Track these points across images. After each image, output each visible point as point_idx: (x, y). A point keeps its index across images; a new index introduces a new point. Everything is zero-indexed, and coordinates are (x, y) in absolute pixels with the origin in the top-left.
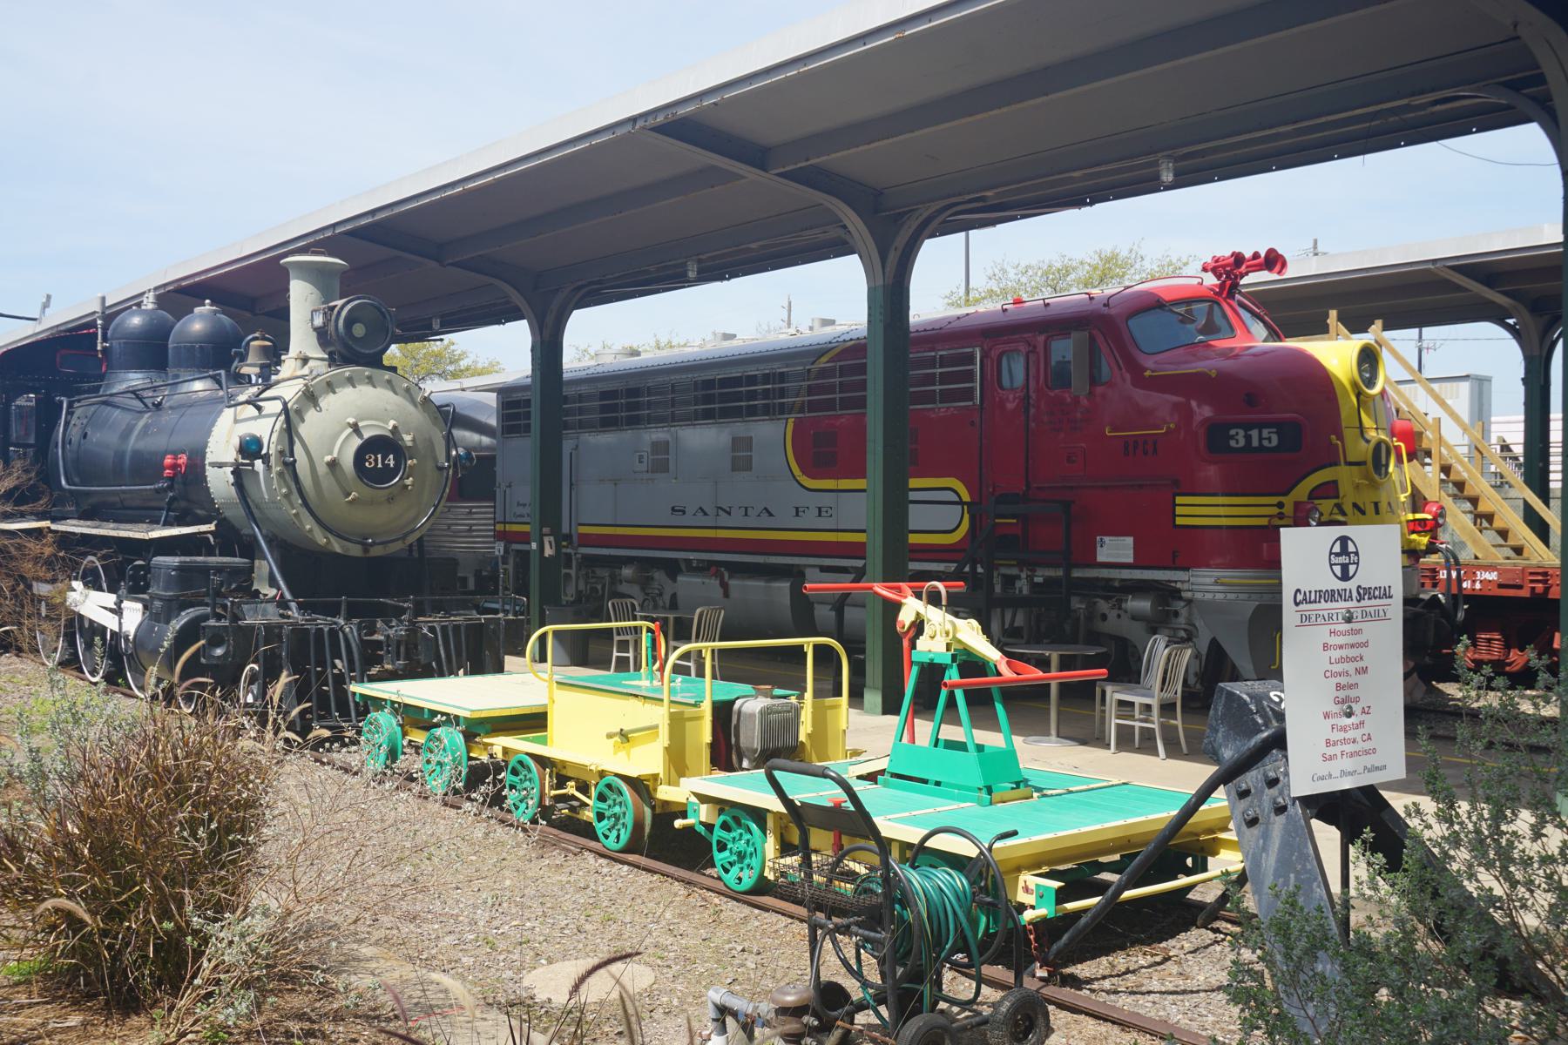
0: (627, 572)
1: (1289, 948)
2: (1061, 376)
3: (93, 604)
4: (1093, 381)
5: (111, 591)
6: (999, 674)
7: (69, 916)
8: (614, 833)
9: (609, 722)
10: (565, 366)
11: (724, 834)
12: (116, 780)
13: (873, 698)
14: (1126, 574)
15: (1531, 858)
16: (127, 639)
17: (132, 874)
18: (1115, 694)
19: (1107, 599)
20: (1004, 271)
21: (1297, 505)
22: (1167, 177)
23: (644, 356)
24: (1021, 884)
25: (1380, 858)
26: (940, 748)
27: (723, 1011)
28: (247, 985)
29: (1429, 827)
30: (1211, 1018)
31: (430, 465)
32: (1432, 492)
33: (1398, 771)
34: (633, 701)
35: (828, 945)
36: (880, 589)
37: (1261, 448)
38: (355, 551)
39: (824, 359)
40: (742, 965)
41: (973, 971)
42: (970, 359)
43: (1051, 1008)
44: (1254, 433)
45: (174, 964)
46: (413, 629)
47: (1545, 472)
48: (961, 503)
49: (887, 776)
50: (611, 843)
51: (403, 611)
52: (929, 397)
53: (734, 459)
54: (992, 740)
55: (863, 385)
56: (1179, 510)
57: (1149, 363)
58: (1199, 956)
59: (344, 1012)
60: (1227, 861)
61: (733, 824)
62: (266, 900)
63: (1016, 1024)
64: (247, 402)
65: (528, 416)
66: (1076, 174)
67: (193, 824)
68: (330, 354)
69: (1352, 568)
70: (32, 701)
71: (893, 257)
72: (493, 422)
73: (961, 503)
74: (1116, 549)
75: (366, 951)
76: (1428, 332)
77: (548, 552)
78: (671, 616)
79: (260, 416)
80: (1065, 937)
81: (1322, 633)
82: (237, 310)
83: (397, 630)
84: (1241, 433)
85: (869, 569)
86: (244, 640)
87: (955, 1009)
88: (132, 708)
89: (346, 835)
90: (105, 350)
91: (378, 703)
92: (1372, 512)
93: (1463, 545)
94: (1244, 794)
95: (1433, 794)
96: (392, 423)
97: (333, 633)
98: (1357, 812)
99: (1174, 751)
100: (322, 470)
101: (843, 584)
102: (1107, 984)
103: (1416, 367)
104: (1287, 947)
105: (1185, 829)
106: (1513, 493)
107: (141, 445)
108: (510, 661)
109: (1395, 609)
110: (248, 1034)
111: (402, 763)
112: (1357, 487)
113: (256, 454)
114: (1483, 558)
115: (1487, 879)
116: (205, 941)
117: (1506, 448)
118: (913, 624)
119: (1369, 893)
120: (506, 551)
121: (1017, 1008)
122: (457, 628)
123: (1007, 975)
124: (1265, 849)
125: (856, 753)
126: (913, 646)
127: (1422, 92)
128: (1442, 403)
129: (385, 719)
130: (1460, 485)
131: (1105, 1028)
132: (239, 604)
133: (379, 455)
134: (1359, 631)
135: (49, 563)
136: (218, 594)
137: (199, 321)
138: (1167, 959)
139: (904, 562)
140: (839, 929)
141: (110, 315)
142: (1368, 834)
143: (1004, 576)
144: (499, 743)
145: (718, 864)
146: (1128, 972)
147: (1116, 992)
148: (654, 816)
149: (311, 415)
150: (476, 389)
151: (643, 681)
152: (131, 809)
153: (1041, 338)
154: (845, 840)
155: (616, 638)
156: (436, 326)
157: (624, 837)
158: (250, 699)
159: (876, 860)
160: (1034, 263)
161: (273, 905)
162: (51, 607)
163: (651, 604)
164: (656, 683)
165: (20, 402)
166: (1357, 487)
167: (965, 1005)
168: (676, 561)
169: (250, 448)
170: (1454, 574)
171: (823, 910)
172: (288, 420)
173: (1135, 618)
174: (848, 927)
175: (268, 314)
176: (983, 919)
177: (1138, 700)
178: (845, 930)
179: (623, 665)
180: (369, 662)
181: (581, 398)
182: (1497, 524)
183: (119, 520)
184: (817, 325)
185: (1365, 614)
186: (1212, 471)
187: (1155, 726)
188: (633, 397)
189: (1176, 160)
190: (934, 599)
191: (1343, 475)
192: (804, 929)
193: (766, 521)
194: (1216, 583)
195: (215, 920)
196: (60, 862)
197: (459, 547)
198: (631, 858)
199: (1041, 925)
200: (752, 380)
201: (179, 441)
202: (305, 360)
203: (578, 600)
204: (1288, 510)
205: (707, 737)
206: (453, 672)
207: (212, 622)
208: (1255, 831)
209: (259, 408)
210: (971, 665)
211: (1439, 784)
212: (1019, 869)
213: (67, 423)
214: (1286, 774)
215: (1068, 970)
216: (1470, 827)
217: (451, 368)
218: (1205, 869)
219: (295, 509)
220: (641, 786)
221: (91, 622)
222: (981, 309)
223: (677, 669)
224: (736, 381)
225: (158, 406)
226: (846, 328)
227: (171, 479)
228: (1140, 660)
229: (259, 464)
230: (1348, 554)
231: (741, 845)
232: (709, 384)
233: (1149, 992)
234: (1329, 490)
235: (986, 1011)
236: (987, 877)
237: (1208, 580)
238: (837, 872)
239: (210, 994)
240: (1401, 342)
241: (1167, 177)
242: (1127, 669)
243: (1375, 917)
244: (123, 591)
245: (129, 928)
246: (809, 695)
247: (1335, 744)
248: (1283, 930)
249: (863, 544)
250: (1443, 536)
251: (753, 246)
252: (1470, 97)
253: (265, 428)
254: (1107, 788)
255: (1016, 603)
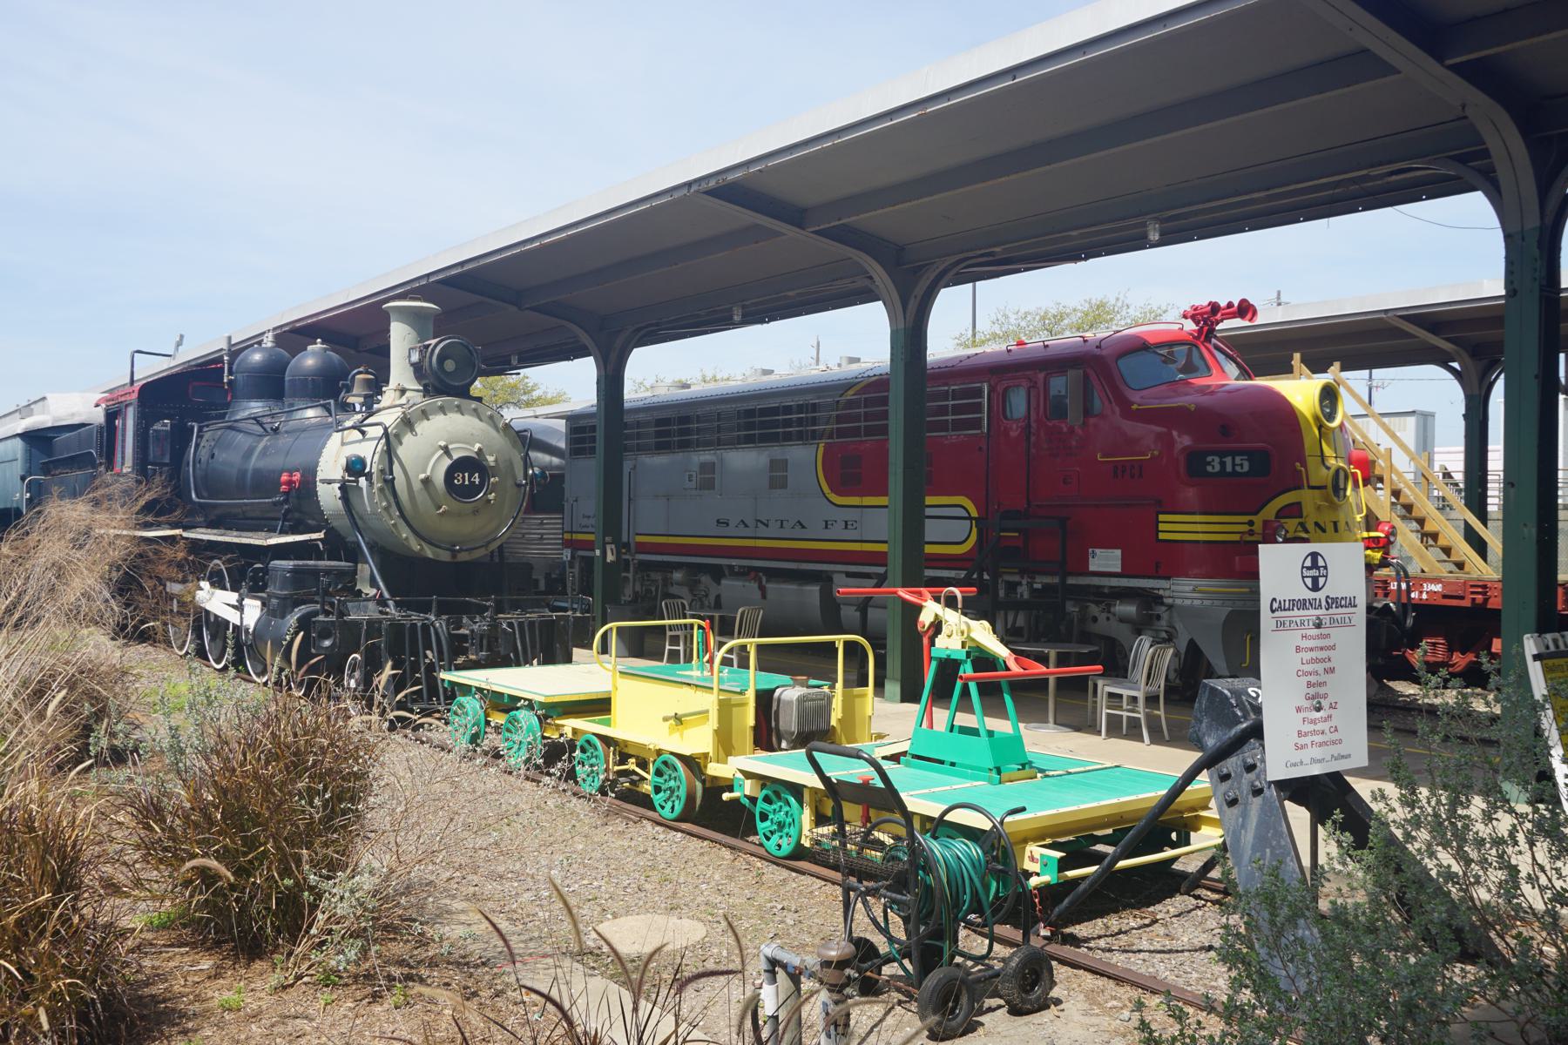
0: (677, 576)
1: (1273, 915)
2: (1059, 409)
3: (217, 601)
4: (1087, 412)
5: (233, 590)
6: (1008, 669)
7: (203, 872)
8: (670, 804)
9: (666, 707)
10: (626, 397)
11: (766, 806)
12: (244, 755)
13: (893, 688)
14: (1115, 582)
15: (1483, 840)
16: (247, 630)
17: (256, 837)
18: (1105, 687)
19: (1097, 603)
20: (1007, 317)
21: (1266, 523)
22: (1154, 236)
23: (693, 388)
24: (1027, 854)
25: (1348, 838)
26: (955, 734)
27: (774, 963)
28: (356, 935)
29: (1393, 810)
30: (1195, 975)
31: (510, 483)
32: (1384, 513)
33: (1361, 759)
34: (686, 689)
35: (859, 905)
36: (903, 593)
37: (1234, 473)
38: (445, 556)
39: (851, 392)
40: (782, 922)
41: (986, 930)
42: (979, 393)
43: (1054, 963)
44: (1228, 460)
45: (293, 915)
46: (494, 625)
47: (1483, 497)
48: (970, 518)
49: (908, 757)
50: (666, 813)
51: (486, 609)
52: (943, 426)
53: (771, 478)
54: (1001, 726)
55: (885, 415)
56: (1162, 527)
57: (1135, 397)
58: (1183, 920)
59: (438, 959)
60: (1207, 837)
61: (773, 798)
62: (372, 864)
63: (1024, 978)
64: (353, 427)
65: (593, 439)
66: (1074, 233)
67: (311, 793)
68: (425, 386)
69: (1322, 581)
70: (165, 684)
71: (913, 305)
72: (562, 445)
73: (970, 518)
74: (1107, 560)
75: (457, 905)
76: (1378, 373)
77: (610, 558)
78: (717, 615)
79: (364, 439)
80: (1066, 901)
81: (1294, 637)
82: (345, 347)
83: (481, 625)
84: (1217, 459)
85: (890, 575)
86: (350, 635)
87: (970, 963)
88: (254, 692)
89: (440, 799)
90: (230, 382)
91: (466, 689)
92: (1333, 530)
93: (1410, 559)
94: (1225, 778)
95: (1398, 782)
96: (478, 446)
97: (425, 628)
98: (1325, 795)
99: (1157, 738)
100: (417, 486)
101: (866, 589)
102: (1102, 943)
103: (1366, 400)
104: (1272, 914)
105: (1173, 807)
106: (1453, 515)
107: (262, 464)
108: (577, 652)
109: (1360, 616)
110: (356, 977)
111: (486, 744)
112: (1319, 508)
113: (361, 473)
114: (1430, 574)
115: (1445, 857)
116: (319, 896)
117: (1447, 475)
118: (932, 624)
119: (1339, 867)
120: (573, 557)
121: (1024, 964)
122: (532, 624)
123: (1017, 935)
124: (1243, 826)
125: (880, 736)
126: (932, 644)
127: (1381, 164)
128: (1393, 436)
129: (472, 704)
130: (1408, 508)
131: (1101, 982)
132: (344, 602)
133: (467, 474)
134: (1327, 636)
135: (180, 566)
136: (326, 593)
137: (311, 358)
138: (1155, 922)
139: (923, 570)
140: (869, 892)
141: (236, 351)
142: (1338, 815)
143: (1008, 582)
144: (570, 724)
145: (761, 833)
146: (1120, 932)
147: (1110, 950)
148: (705, 790)
149: (408, 439)
150: (547, 416)
151: (695, 672)
152: (256, 776)
153: (1041, 376)
154: (872, 812)
155: (669, 633)
156: (514, 362)
157: (678, 808)
158: (353, 684)
159: (902, 832)
160: (1032, 308)
161: (376, 864)
162: (182, 604)
163: (700, 604)
164: (706, 673)
165: (157, 427)
166: (1319, 508)
167: (978, 960)
168: (720, 567)
169: (355, 467)
170: (1404, 586)
171: (856, 876)
172: (388, 443)
173: (1122, 620)
174: (877, 890)
175: (370, 351)
176: (994, 884)
177: (1126, 693)
178: (873, 892)
179: (674, 657)
180: (457, 652)
181: (639, 424)
182: (1442, 542)
183: (241, 528)
184: (844, 363)
185: (1332, 621)
186: (1190, 494)
187: (1141, 716)
188: (686, 424)
189: (1162, 221)
190: (951, 603)
191: (1307, 497)
192: (839, 891)
193: (798, 532)
194: (1194, 591)
195: (329, 878)
196: (196, 825)
197: (533, 552)
198: (684, 826)
199: (1045, 889)
200: (788, 410)
201: (295, 460)
202: (403, 391)
203: (634, 601)
204: (1258, 527)
205: (751, 721)
206: (528, 662)
207: (321, 618)
208: (1235, 810)
209: (363, 433)
210: (983, 661)
211: (1402, 773)
212: (1025, 841)
213: (197, 445)
214: (1263, 761)
215: (1068, 930)
216: (1430, 810)
217: (525, 398)
218: (1188, 843)
219: (393, 519)
220: (693, 764)
221: (216, 617)
222: (989, 348)
223: (726, 662)
224: (774, 411)
225: (276, 430)
226: (869, 366)
227: (287, 493)
228: (1127, 657)
229: (363, 481)
230: (1318, 568)
231: (781, 816)
232: (750, 413)
233: (1140, 951)
234: (1294, 510)
235: (998, 966)
236: (998, 848)
237: (1187, 588)
238: (869, 842)
239: (323, 943)
240: (1356, 380)
241: (1154, 236)
242: (1117, 667)
243: (1345, 889)
244: (244, 590)
245: (254, 883)
246: (839, 685)
247: (1306, 734)
248: (1269, 900)
249: (885, 554)
250: (1394, 552)
251: (791, 293)
252: (1422, 169)
253: (369, 450)
254: (1102, 771)
255: (1018, 606)
